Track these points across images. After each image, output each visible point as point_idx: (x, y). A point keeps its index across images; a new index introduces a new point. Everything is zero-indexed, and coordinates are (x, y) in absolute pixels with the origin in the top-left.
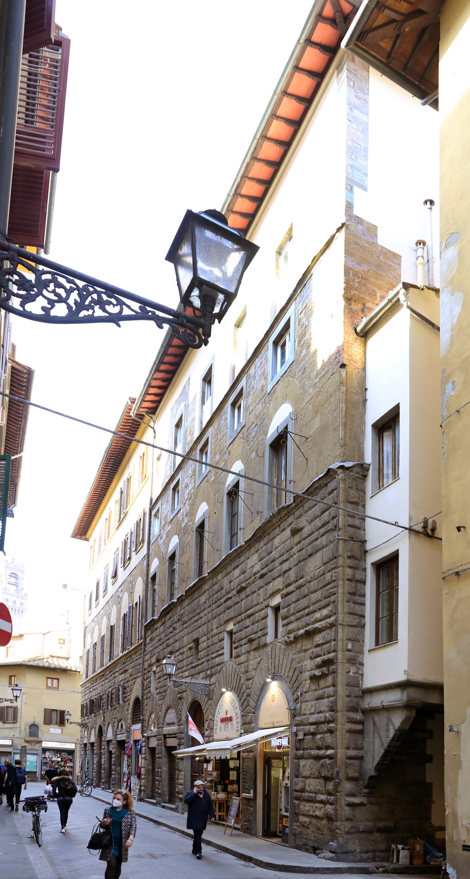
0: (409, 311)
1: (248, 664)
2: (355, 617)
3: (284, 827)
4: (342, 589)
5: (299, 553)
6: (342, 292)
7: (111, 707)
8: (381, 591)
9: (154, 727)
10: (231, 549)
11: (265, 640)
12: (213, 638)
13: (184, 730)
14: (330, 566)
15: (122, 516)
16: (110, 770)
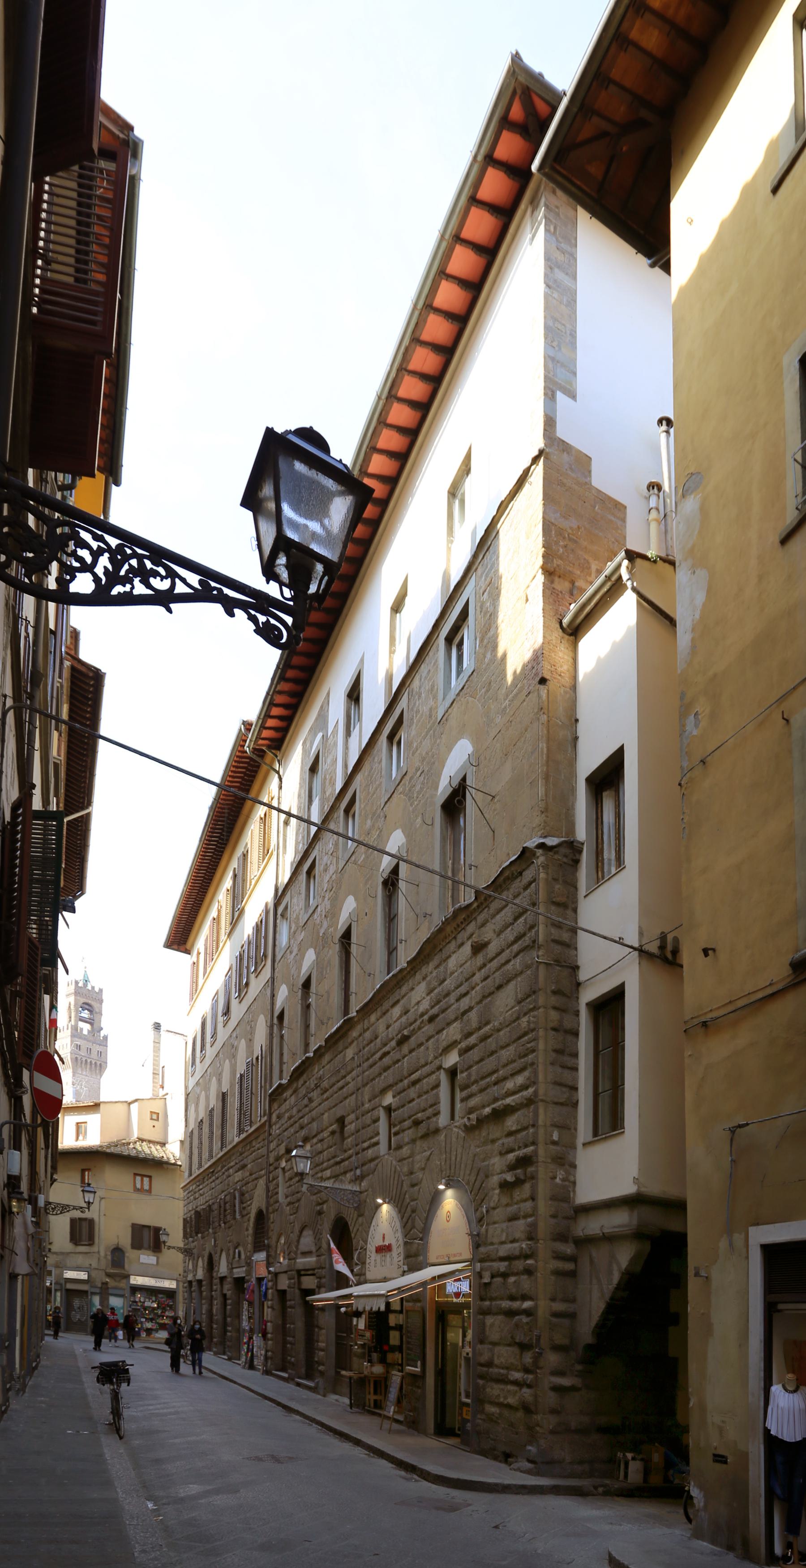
0: (634, 596)
1: (413, 1161)
2: (564, 1089)
4: (544, 1044)
5: (484, 983)
6: (540, 561)
7: (225, 1223)
9: (284, 1258)
10: (388, 974)
11: (437, 1122)
14: (528, 1004)
15: (236, 914)
16: (225, 1324)
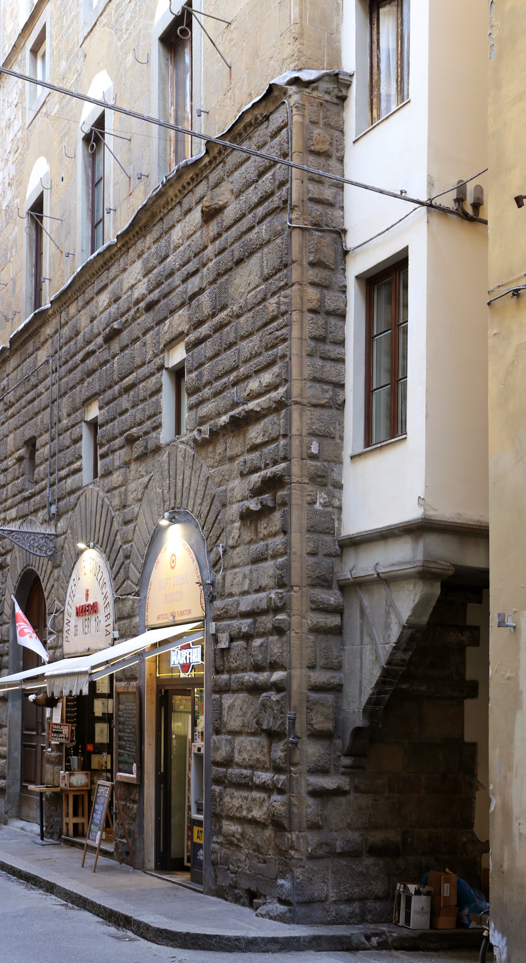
1: (126, 490)
2: (326, 387)
3: (197, 847)
4: (299, 330)
5: (218, 258)
8: (375, 333)
10: (92, 253)
11: (157, 438)
12: (61, 437)
13: (8, 636)
